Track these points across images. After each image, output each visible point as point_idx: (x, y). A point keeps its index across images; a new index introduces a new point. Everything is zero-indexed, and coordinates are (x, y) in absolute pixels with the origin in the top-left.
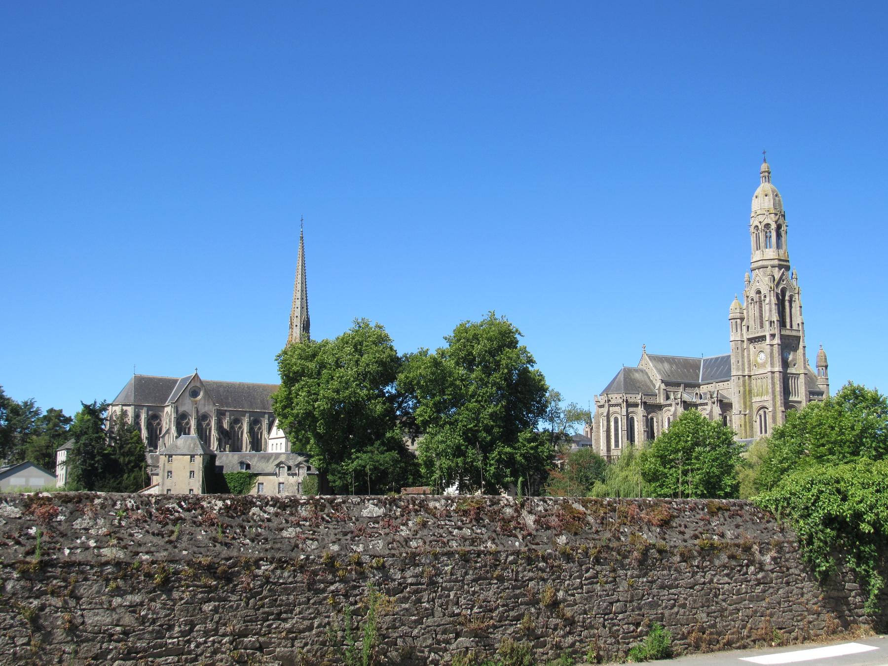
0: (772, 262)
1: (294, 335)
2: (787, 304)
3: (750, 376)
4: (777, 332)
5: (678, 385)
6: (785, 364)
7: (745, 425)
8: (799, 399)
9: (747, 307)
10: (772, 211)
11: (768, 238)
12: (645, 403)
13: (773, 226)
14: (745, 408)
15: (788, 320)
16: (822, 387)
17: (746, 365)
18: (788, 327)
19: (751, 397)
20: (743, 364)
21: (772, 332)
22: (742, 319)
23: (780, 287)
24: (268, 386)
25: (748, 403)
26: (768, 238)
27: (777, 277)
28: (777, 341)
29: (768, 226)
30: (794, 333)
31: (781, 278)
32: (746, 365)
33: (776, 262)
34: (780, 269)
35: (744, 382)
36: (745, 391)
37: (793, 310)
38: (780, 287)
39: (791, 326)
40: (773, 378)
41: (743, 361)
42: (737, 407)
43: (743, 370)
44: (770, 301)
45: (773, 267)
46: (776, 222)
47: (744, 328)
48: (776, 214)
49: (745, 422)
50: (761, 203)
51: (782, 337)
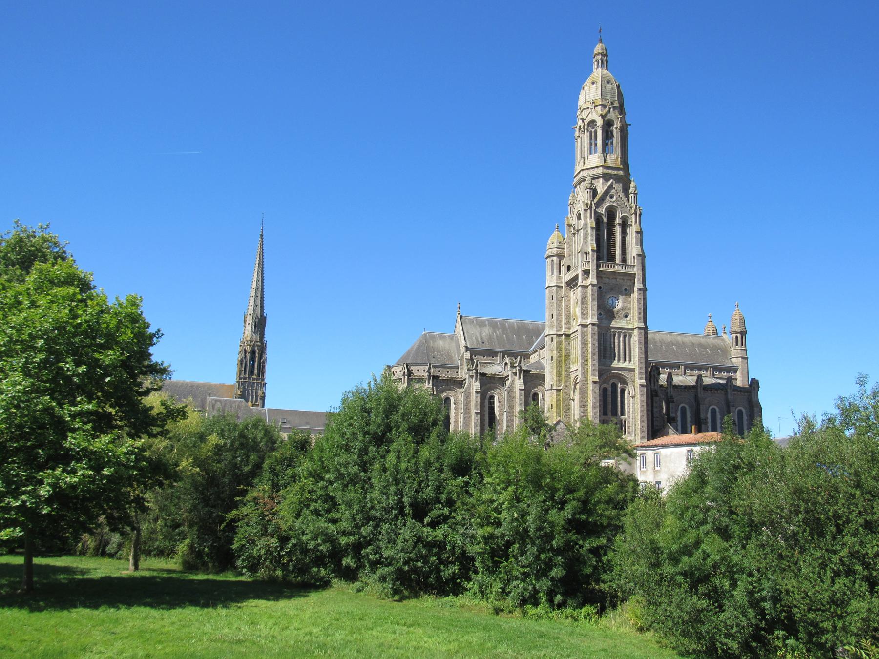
0: (593, 172)
1: (246, 333)
2: (618, 230)
3: (568, 336)
4: (592, 267)
5: (494, 354)
6: (606, 313)
7: (558, 406)
8: (631, 366)
9: (569, 239)
10: (599, 102)
11: (593, 137)
12: (435, 378)
13: (599, 121)
14: (559, 380)
15: (618, 252)
16: (737, 362)
17: (564, 321)
18: (618, 259)
19: (568, 366)
20: (559, 319)
21: (584, 268)
22: (561, 257)
23: (605, 206)
24: (215, 385)
25: (564, 374)
26: (593, 137)
27: (601, 190)
28: (593, 279)
29: (592, 122)
30: (629, 270)
31: (607, 193)
32: (564, 321)
33: (600, 171)
34: (607, 180)
35: (559, 344)
36: (559, 357)
37: (628, 238)
38: (605, 206)
39: (624, 260)
40: (583, 334)
41: (559, 315)
42: (550, 379)
43: (559, 327)
44: (586, 224)
45: (594, 178)
46: (603, 116)
47: (564, 269)
48: (604, 106)
49: (558, 400)
50: (590, 94)
51: (600, 275)
